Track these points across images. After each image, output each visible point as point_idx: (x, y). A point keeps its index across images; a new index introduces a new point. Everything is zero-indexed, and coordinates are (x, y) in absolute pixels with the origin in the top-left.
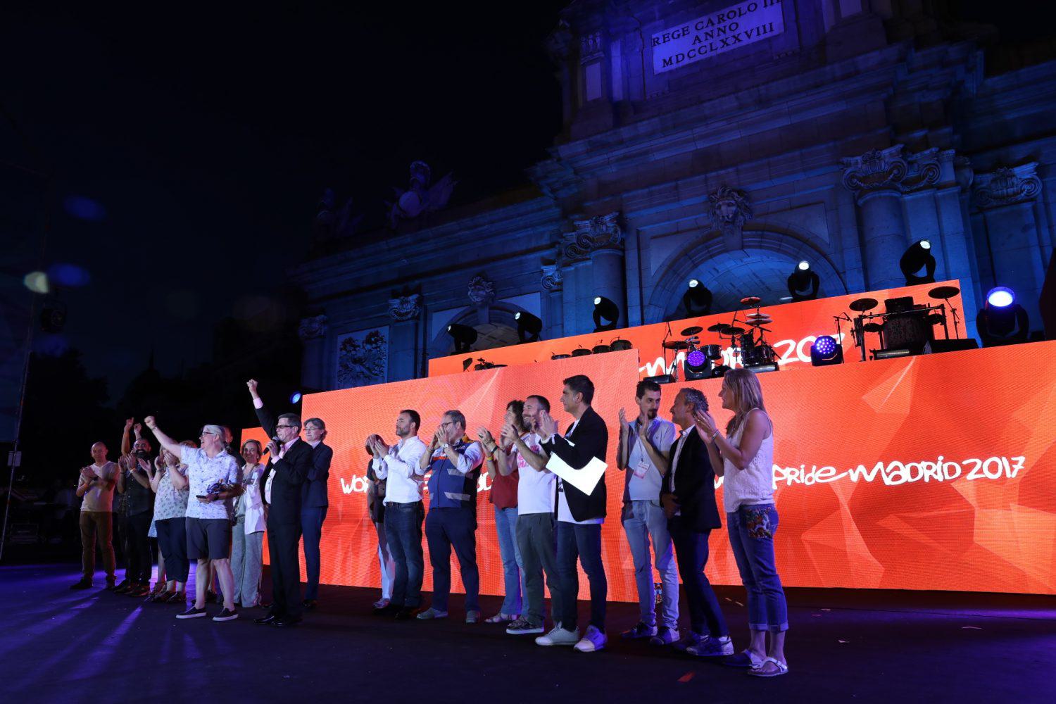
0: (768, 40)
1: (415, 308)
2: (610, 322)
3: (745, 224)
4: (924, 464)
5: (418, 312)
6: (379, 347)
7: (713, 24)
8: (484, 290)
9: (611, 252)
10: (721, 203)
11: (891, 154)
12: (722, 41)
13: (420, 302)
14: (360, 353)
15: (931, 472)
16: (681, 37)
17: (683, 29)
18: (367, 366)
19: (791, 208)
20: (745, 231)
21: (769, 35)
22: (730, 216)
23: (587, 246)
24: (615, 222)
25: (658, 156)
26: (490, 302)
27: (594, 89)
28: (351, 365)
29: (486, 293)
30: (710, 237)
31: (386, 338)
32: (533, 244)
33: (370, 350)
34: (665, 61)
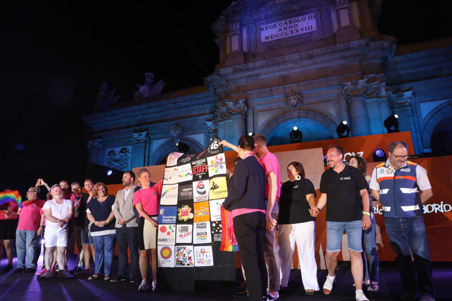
0: (310, 33)
1: (145, 137)
4: (434, 205)
5: (146, 139)
7: (287, 24)
8: (178, 131)
9: (240, 116)
12: (291, 31)
13: (147, 135)
14: (117, 157)
15: (438, 209)
16: (273, 28)
17: (274, 25)
19: (320, 102)
20: (300, 110)
21: (310, 31)
22: (295, 104)
23: (230, 113)
25: (264, 77)
26: (181, 136)
27: (235, 47)
28: (113, 162)
32: (202, 112)
33: (122, 156)
34: (266, 37)
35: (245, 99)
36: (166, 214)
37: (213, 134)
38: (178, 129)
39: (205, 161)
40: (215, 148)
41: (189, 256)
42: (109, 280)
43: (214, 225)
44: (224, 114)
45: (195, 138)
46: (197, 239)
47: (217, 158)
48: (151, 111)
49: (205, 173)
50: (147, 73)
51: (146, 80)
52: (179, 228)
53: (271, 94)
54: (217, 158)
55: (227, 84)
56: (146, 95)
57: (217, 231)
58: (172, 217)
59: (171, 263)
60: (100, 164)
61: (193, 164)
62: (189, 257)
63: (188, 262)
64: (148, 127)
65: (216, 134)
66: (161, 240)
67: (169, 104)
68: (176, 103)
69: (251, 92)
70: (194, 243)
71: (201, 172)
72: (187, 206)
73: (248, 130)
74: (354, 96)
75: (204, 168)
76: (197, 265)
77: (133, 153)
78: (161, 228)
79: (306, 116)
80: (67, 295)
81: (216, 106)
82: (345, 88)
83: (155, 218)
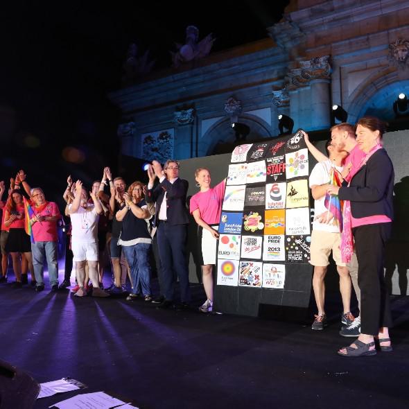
13: (194, 114)
14: (156, 145)
23: (307, 77)
25: (356, 19)
28: (151, 152)
32: (267, 78)
36: (229, 221)
37: (283, 108)
40: (296, 142)
42: (151, 300)
43: (289, 240)
44: (298, 79)
45: (258, 115)
46: (268, 256)
47: (297, 155)
48: (197, 79)
54: (297, 155)
55: (302, 34)
56: (189, 58)
57: (292, 247)
58: (236, 226)
60: (134, 156)
61: (268, 161)
63: (254, 282)
64: (194, 103)
65: (287, 108)
68: (230, 67)
70: (264, 259)
72: (257, 214)
73: (333, 101)
76: (266, 286)
78: (222, 239)
83: (216, 228)
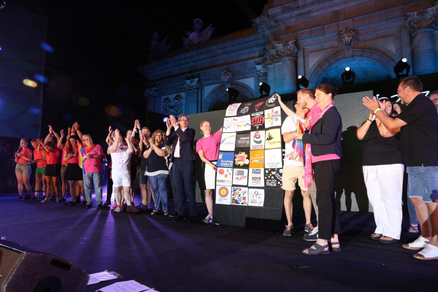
1: (197, 84)
2: (266, 93)
3: (355, 45)
6: (181, 101)
8: (228, 76)
9: (290, 58)
10: (345, 35)
11: (432, 10)
13: (199, 81)
14: (172, 104)
18: (175, 109)
19: (377, 38)
20: (355, 49)
22: (349, 41)
23: (280, 56)
24: (294, 44)
25: (315, 14)
28: (168, 109)
29: (229, 77)
30: (338, 52)
31: (184, 98)
32: (251, 56)
35: (295, 40)
36: (224, 158)
37: (263, 77)
38: (228, 74)
39: (262, 113)
40: (272, 102)
41: (244, 197)
42: (169, 215)
44: (273, 57)
46: (252, 183)
47: (273, 111)
49: (262, 124)
50: (195, 19)
51: (195, 26)
52: (235, 171)
53: (322, 33)
54: (273, 111)
55: (277, 24)
56: (196, 42)
58: (229, 162)
59: (227, 201)
62: (243, 197)
65: (265, 77)
66: (220, 181)
67: (218, 49)
68: (225, 48)
69: (301, 32)
70: (249, 186)
71: (259, 123)
72: (244, 153)
74: (420, 27)
75: (262, 120)
76: (250, 204)
77: (187, 100)
78: (220, 171)
79: (361, 55)
80: (134, 227)
81: (265, 49)
82: (409, 20)
83: (215, 163)
